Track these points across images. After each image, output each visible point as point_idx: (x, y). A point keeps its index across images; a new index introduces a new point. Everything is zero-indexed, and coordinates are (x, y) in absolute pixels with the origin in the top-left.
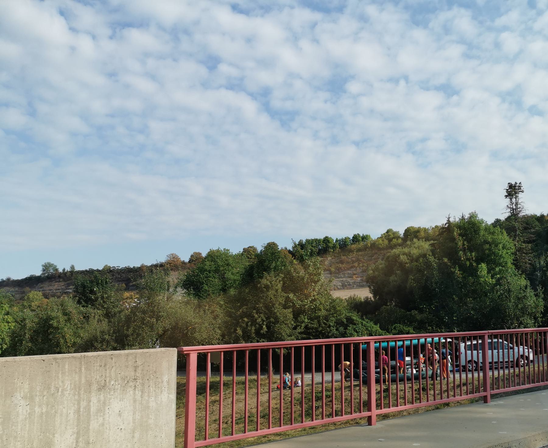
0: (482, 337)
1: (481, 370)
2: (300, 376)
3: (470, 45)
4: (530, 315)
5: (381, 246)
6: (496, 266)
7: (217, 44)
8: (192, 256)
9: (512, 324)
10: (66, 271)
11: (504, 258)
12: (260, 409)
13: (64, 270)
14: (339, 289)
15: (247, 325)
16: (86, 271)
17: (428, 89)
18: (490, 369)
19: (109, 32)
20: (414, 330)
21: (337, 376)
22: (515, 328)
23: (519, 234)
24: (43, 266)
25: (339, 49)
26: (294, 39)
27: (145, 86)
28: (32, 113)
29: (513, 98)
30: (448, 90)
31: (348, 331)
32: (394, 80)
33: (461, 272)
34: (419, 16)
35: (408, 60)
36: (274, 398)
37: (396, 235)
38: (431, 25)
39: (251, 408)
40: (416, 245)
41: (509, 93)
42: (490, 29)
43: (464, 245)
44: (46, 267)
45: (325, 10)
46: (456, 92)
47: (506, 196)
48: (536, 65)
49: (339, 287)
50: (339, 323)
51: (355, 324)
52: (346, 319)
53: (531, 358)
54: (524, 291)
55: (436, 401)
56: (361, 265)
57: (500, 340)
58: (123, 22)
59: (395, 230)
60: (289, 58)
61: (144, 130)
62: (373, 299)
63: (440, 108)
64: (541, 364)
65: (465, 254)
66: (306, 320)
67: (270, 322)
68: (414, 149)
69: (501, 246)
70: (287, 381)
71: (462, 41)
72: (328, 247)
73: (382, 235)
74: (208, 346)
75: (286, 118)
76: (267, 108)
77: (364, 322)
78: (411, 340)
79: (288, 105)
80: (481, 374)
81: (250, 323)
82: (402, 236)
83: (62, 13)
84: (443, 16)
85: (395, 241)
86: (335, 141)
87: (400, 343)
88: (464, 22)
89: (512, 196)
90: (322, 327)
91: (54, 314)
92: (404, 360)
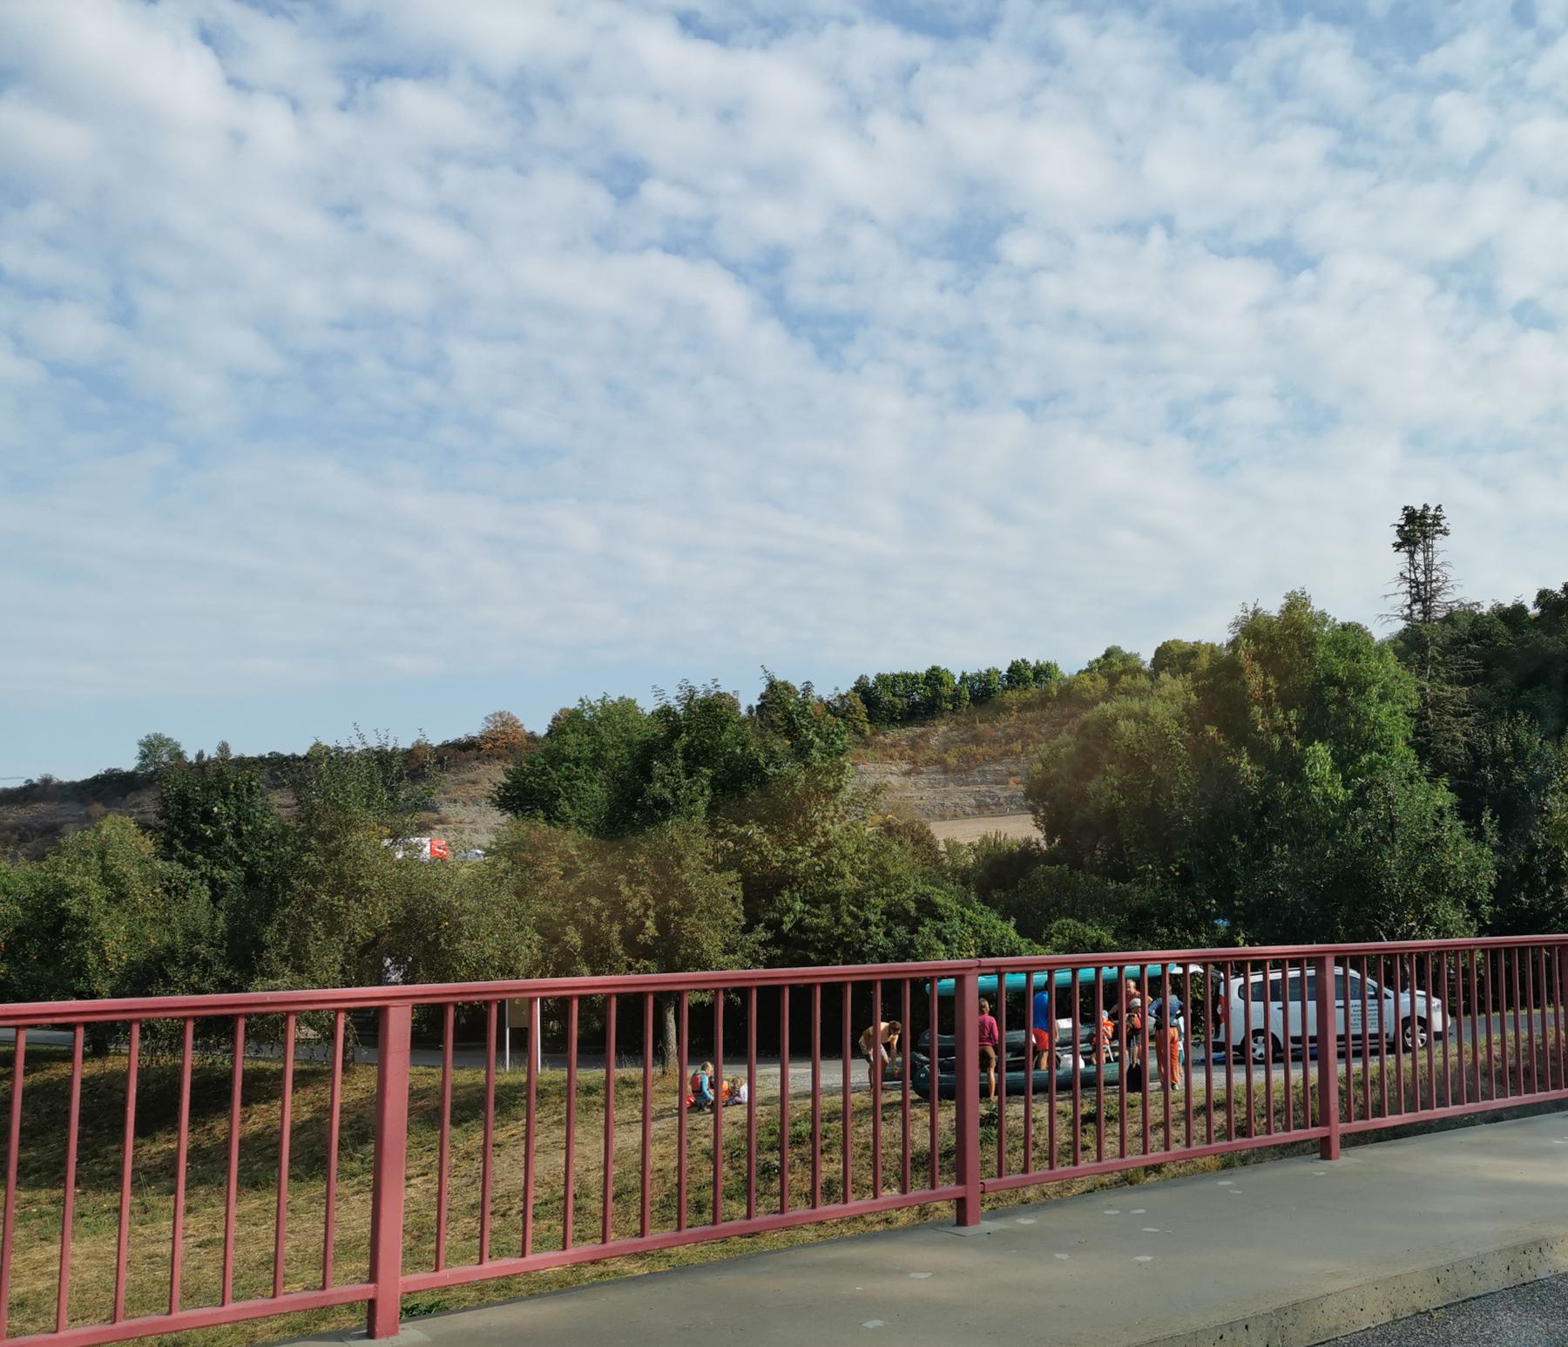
0: (1317, 961)
1: (1313, 1058)
2: (776, 1070)
3: (1349, 131)
4: (1456, 895)
5: (1087, 696)
6: (1363, 752)
7: (638, 125)
8: (555, 719)
9: (1398, 922)
10: (205, 759)
11: (1382, 727)
12: (615, 1170)
13: (200, 755)
14: (967, 815)
15: (598, 917)
16: (262, 759)
17: (1228, 254)
18: (1341, 1055)
19: (337, 90)
20: (1115, 937)
21: (860, 1073)
22: (1406, 936)
23: (1434, 658)
24: (141, 744)
25: (977, 139)
26: (853, 111)
27: (438, 242)
28: (125, 316)
29: (1470, 280)
30: (1287, 256)
31: (917, 939)
32: (1134, 228)
33: (1256, 769)
34: (1204, 45)
35: (1174, 171)
36: (661, 1140)
37: (1130, 664)
38: (1238, 72)
39: (588, 1170)
40: (1165, 692)
41: (1460, 266)
42: (1404, 84)
43: (1266, 687)
44: (151, 747)
45: (940, 28)
46: (1310, 264)
47: (1398, 546)
48: (1533, 187)
49: (968, 810)
50: (894, 915)
51: (941, 919)
52: (917, 901)
53: (1437, 1024)
54: (1436, 824)
55: (1128, 1158)
56: (1031, 748)
57: (1353, 973)
58: (377, 63)
59: (1127, 649)
60: (840, 164)
61: (435, 366)
62: (1043, 844)
63: (1264, 306)
64: (1467, 1045)
65: (1269, 713)
66: (798, 906)
67: (667, 911)
68: (1191, 422)
69: (1375, 691)
70: (706, 1087)
71: (1326, 118)
72: (937, 695)
73: (1090, 663)
74: (330, 990)
75: (830, 335)
76: (776, 305)
77: (969, 913)
78: (1029, 974)
79: (837, 299)
80: (1314, 1072)
81: (607, 912)
82: (1147, 666)
83: (207, 37)
84: (1273, 47)
85: (1126, 680)
86: (967, 399)
87: (1040, 978)
88: (1330, 64)
89: (1416, 544)
90: (844, 925)
91: (74, 881)
92: (1050, 1028)
